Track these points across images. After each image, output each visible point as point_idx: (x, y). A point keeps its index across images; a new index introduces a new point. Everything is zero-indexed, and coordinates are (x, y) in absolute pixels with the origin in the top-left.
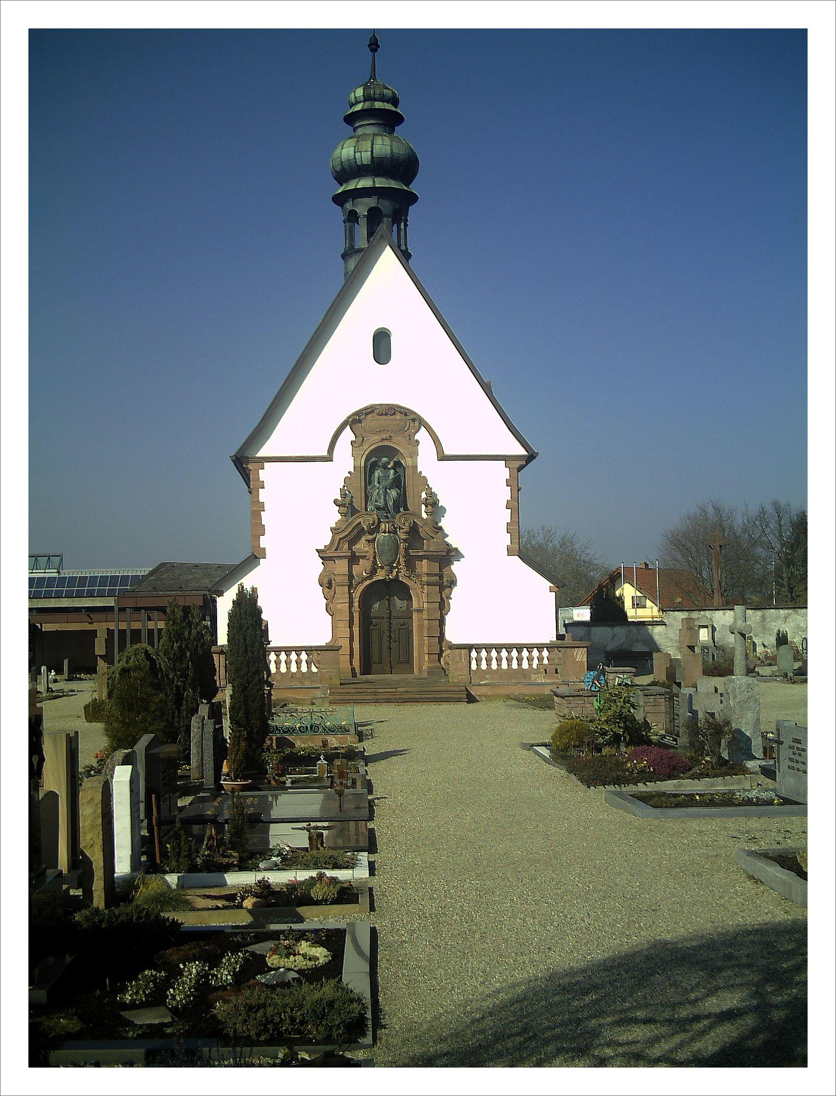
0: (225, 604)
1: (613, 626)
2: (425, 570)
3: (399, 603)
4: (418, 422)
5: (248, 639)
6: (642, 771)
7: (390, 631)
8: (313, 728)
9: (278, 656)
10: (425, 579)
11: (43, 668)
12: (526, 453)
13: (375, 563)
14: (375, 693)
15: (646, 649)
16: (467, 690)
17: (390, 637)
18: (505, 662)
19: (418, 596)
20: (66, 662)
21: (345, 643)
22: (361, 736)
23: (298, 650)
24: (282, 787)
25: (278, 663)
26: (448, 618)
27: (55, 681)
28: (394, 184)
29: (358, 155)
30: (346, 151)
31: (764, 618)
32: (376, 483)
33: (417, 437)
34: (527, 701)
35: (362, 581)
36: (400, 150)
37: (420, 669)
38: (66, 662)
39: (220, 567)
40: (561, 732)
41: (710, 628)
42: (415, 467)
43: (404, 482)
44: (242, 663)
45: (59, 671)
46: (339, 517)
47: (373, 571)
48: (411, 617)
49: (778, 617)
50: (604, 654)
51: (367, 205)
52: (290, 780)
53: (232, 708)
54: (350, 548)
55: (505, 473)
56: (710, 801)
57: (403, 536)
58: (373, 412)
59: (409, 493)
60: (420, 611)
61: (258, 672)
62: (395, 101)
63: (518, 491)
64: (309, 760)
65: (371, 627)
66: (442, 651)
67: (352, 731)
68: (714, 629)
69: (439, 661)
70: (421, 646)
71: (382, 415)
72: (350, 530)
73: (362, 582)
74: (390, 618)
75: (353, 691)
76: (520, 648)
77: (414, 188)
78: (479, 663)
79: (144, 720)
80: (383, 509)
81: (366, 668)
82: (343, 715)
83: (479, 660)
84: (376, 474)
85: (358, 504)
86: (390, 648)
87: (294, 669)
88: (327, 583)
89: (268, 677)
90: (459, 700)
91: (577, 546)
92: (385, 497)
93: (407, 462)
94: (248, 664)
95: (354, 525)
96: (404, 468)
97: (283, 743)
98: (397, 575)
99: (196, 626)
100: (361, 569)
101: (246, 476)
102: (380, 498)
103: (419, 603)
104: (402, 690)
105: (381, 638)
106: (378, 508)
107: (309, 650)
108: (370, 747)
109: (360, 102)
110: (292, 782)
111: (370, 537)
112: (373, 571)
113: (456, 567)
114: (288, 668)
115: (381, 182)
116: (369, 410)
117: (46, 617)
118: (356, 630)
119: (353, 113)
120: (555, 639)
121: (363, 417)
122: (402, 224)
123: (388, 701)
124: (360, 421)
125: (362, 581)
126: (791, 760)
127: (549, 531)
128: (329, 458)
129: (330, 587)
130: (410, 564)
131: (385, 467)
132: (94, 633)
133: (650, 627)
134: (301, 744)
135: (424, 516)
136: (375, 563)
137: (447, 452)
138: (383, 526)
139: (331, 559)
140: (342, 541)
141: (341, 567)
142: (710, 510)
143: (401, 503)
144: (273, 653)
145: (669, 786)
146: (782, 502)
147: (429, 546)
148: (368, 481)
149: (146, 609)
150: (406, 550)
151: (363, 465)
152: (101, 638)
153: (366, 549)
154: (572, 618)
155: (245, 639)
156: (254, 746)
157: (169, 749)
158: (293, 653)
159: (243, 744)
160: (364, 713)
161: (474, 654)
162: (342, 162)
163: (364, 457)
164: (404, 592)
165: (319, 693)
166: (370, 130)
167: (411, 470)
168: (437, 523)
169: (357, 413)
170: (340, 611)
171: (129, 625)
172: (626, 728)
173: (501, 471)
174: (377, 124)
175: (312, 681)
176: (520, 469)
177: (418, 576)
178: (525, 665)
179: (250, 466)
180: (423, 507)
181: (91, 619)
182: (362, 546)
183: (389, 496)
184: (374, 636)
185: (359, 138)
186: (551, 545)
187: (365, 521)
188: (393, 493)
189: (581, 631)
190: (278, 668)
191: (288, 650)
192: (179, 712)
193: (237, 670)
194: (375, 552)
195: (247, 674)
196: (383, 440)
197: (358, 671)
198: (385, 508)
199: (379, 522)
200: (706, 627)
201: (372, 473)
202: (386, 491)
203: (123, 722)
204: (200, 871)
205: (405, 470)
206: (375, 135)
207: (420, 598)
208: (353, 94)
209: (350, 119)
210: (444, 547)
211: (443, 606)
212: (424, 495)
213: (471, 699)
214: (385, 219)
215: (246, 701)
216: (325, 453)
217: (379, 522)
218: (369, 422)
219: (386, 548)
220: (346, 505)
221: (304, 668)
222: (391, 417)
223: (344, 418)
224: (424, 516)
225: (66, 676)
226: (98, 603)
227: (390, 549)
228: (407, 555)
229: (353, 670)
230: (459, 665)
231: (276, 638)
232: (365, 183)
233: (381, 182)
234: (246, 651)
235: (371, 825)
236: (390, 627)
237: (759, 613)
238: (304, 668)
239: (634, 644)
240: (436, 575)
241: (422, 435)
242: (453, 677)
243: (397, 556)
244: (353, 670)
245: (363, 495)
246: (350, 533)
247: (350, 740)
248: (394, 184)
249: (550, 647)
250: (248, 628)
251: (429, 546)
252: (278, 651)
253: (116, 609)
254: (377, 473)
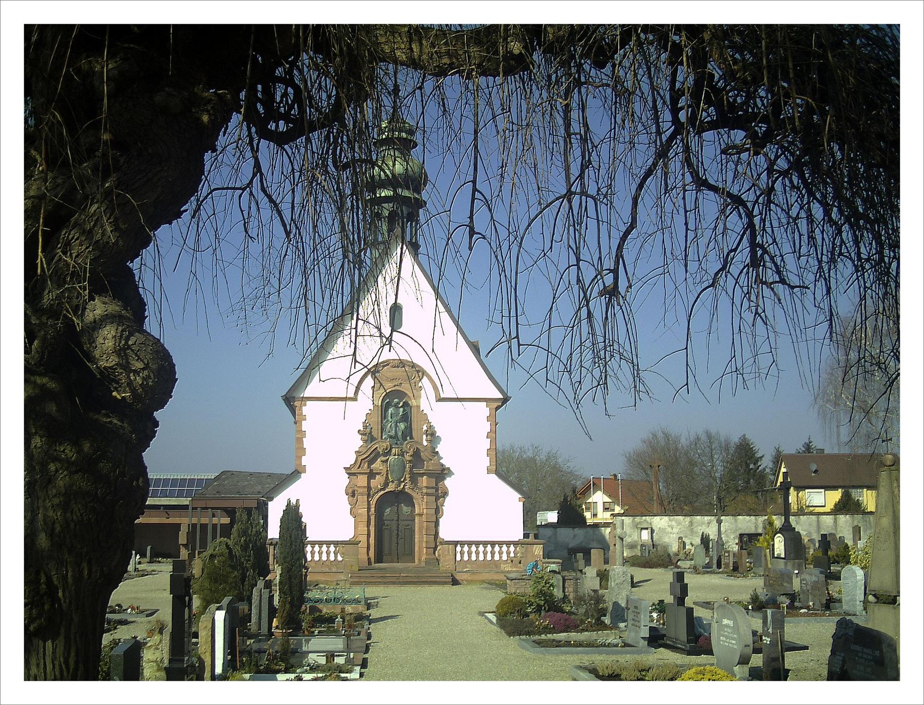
0: (276, 510)
1: (574, 528)
2: (425, 484)
3: (405, 509)
4: (420, 372)
5: (293, 536)
6: (546, 627)
7: (398, 530)
8: (336, 600)
10: (425, 491)
13: (387, 478)
16: (452, 575)
18: (481, 555)
19: (419, 504)
20: (149, 548)
21: (363, 539)
22: (369, 607)
23: (328, 543)
24: (312, 634)
25: (313, 553)
26: (442, 521)
27: (140, 563)
31: (691, 523)
34: (496, 585)
35: (377, 492)
37: (420, 560)
38: (149, 548)
39: (269, 475)
40: (503, 603)
41: (649, 530)
42: (418, 407)
43: (411, 417)
44: (288, 553)
45: (143, 555)
46: (361, 443)
47: (386, 484)
48: (414, 520)
49: (703, 523)
50: (567, 550)
52: (317, 631)
53: (280, 583)
54: (369, 467)
55: (487, 412)
56: (579, 644)
58: (388, 365)
59: (414, 426)
60: (420, 515)
61: (299, 559)
63: (496, 425)
64: (331, 620)
65: (384, 527)
66: (436, 547)
67: (363, 603)
68: (652, 531)
69: (434, 553)
70: (421, 542)
71: (395, 367)
74: (398, 520)
76: (493, 544)
78: (463, 554)
79: (224, 589)
80: (394, 438)
81: (379, 559)
82: (356, 592)
83: (462, 553)
84: (390, 412)
85: (375, 433)
86: (397, 543)
87: (324, 558)
88: (352, 493)
89: (305, 563)
90: (445, 583)
91: (560, 460)
93: (413, 402)
94: (292, 554)
96: (411, 407)
97: (313, 609)
99: (256, 527)
100: (377, 482)
101: (293, 410)
102: (392, 430)
103: (420, 509)
104: (405, 575)
105: (391, 537)
106: (391, 437)
107: (336, 543)
108: (374, 613)
110: (319, 632)
112: (386, 484)
113: (448, 482)
114: (320, 557)
120: (522, 537)
123: (393, 583)
125: (377, 492)
126: (633, 620)
128: (354, 399)
129: (353, 496)
130: (414, 479)
131: (396, 406)
132: (178, 526)
133: (603, 528)
134: (326, 610)
135: (425, 443)
136: (387, 478)
138: (393, 451)
141: (362, 480)
142: (660, 434)
144: (309, 546)
145: (562, 636)
146: (713, 432)
147: (428, 466)
148: (384, 416)
149: (212, 508)
150: (411, 468)
151: (380, 404)
152: (183, 531)
154: (546, 520)
156: (294, 609)
157: (243, 607)
159: (288, 606)
160: (371, 591)
161: (459, 548)
163: (381, 399)
164: (409, 500)
165: (342, 577)
168: (434, 449)
170: (361, 515)
171: (199, 520)
172: (546, 601)
173: (483, 410)
175: (337, 568)
176: (497, 408)
178: (497, 557)
179: (296, 403)
180: (424, 436)
182: (377, 465)
183: (399, 429)
184: (386, 534)
186: (539, 459)
187: (381, 446)
188: (402, 426)
189: (549, 532)
190: (313, 556)
191: (321, 543)
192: (243, 586)
193: (285, 558)
195: (291, 560)
197: (373, 560)
198: (395, 437)
200: (647, 529)
201: (386, 410)
202: (396, 424)
203: (211, 590)
204: (262, 673)
207: (421, 506)
210: (439, 468)
211: (438, 512)
213: (455, 582)
215: (290, 578)
216: (352, 395)
220: (367, 435)
221: (332, 558)
224: (425, 443)
225: (148, 559)
226: (173, 501)
227: (399, 469)
228: (411, 472)
229: (369, 559)
230: (448, 557)
231: (311, 535)
234: (291, 544)
235: (366, 656)
236: (398, 527)
237: (688, 519)
238: (332, 558)
239: (591, 542)
240: (433, 488)
242: (443, 566)
243: (403, 475)
244: (369, 559)
245: (380, 427)
247: (361, 608)
249: (516, 544)
250: (293, 529)
251: (428, 466)
252: (313, 543)
253: (190, 508)
254: (391, 410)
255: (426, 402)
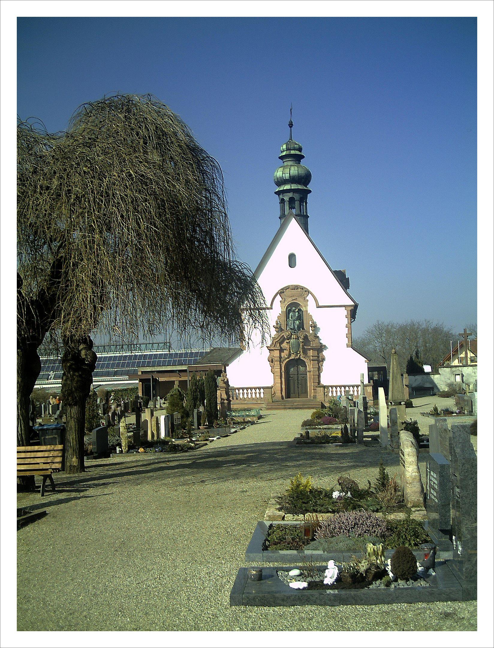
3: (302, 368)
4: (308, 292)
9: (247, 391)
10: (311, 358)
11: (159, 397)
12: (354, 304)
13: (290, 352)
14: (285, 405)
15: (431, 386)
17: (298, 382)
23: (259, 388)
27: (164, 403)
28: (300, 187)
29: (284, 175)
30: (279, 174)
32: (291, 319)
33: (307, 298)
36: (302, 172)
37: (310, 396)
41: (461, 375)
42: (307, 311)
46: (276, 333)
47: (290, 355)
48: (307, 374)
51: (288, 196)
54: (280, 346)
57: (301, 340)
58: (289, 288)
60: (310, 372)
62: (300, 149)
68: (463, 376)
71: (292, 289)
72: (279, 338)
73: (285, 360)
75: (276, 404)
77: (310, 187)
80: (293, 329)
81: (288, 396)
88: (271, 361)
92: (294, 324)
93: (303, 309)
94: (211, 393)
95: (281, 336)
98: (300, 357)
100: (284, 354)
102: (292, 325)
106: (291, 329)
109: (285, 151)
111: (288, 341)
113: (325, 353)
115: (294, 186)
116: (287, 288)
117: (160, 375)
118: (283, 380)
119: (282, 156)
121: (284, 291)
122: (304, 203)
124: (283, 292)
127: (429, 322)
130: (305, 352)
131: (294, 311)
135: (311, 332)
136: (290, 352)
137: (320, 305)
138: (293, 336)
139: (272, 350)
140: (276, 343)
141: (277, 353)
143: (301, 326)
147: (313, 344)
148: (287, 317)
151: (285, 311)
153: (287, 346)
155: (210, 385)
158: (262, 389)
162: (277, 178)
163: (286, 307)
164: (304, 364)
165: (264, 406)
166: (290, 163)
167: (305, 312)
169: (282, 289)
170: (277, 371)
174: (292, 160)
177: (309, 357)
180: (311, 328)
181: (180, 375)
182: (285, 345)
185: (284, 167)
187: (286, 334)
188: (297, 322)
194: (290, 347)
196: (293, 300)
197: (284, 397)
198: (294, 329)
199: (292, 334)
200: (459, 375)
201: (289, 314)
205: (303, 312)
206: (291, 166)
207: (310, 366)
208: (282, 147)
209: (281, 158)
211: (319, 369)
212: (311, 323)
214: (296, 202)
215: (210, 404)
217: (292, 334)
218: (288, 292)
219: (294, 345)
222: (297, 290)
223: (276, 292)
224: (311, 332)
228: (303, 348)
229: (282, 396)
232: (287, 187)
233: (294, 186)
240: (316, 356)
241: (309, 297)
244: (282, 396)
246: (280, 339)
248: (300, 187)
251: (313, 344)
255: (311, 309)
